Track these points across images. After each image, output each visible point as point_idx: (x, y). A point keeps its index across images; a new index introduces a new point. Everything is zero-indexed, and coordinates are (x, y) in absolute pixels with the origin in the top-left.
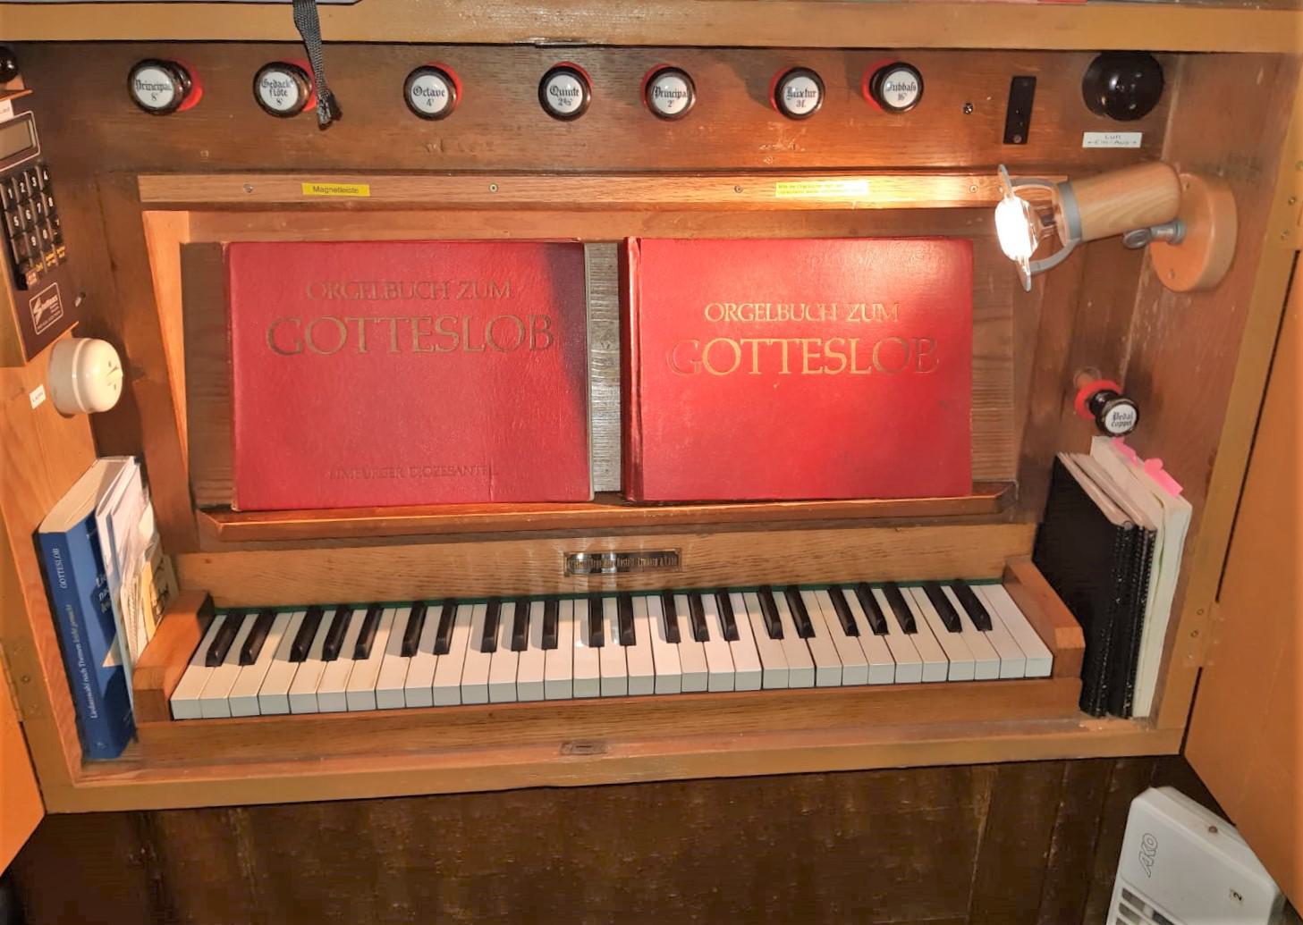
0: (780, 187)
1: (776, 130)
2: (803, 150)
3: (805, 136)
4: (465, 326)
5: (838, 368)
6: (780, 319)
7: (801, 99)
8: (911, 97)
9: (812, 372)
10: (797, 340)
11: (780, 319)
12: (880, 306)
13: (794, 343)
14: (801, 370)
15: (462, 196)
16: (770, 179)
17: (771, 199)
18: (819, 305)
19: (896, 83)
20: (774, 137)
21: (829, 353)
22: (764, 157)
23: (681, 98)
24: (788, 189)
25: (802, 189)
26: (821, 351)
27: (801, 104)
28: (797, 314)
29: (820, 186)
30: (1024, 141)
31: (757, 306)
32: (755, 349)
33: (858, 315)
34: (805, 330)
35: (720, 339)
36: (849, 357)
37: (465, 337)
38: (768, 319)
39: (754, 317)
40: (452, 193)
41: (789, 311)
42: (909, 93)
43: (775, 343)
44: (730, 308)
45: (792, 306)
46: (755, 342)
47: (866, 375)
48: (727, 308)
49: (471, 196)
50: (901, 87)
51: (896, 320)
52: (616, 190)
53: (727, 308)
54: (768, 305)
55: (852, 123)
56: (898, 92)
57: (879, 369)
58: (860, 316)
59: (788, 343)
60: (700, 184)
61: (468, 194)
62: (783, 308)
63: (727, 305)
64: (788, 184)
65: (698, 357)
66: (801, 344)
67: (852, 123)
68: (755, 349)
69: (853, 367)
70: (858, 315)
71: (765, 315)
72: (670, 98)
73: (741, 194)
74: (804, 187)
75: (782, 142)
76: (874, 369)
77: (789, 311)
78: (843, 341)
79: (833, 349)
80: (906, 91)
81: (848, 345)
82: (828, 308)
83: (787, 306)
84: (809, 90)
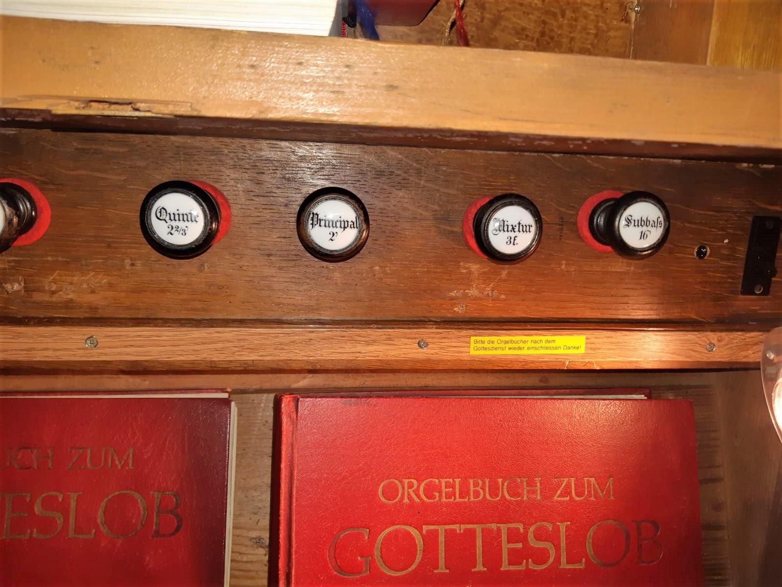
0: (476, 342)
1: (470, 273)
2: (503, 297)
3: (505, 280)
4: (73, 504)
5: (544, 562)
6: (472, 499)
7: (512, 235)
8: (655, 235)
9: (512, 568)
10: (494, 526)
11: (472, 499)
12: (593, 480)
13: (490, 530)
14: (500, 564)
15: (50, 353)
16: (464, 333)
17: (464, 357)
18: (519, 480)
19: (636, 217)
20: (466, 281)
21: (533, 543)
22: (454, 305)
23: (348, 229)
24: (486, 345)
25: (502, 345)
26: (524, 539)
27: (512, 241)
28: (494, 491)
29: (524, 342)
30: (766, 292)
31: (443, 481)
32: (442, 539)
33: (567, 492)
34: (503, 513)
35: (397, 527)
36: (558, 548)
37: (72, 520)
38: (458, 500)
39: (440, 496)
40: (34, 349)
41: (483, 489)
42: (653, 230)
43: (466, 530)
44: (411, 486)
45: (487, 481)
46: (441, 529)
47: (580, 569)
48: (406, 486)
49: (58, 353)
50: (643, 222)
51: (612, 498)
52: (262, 344)
53: (406, 486)
54: (457, 481)
55: (563, 267)
56: (640, 229)
57: (595, 561)
58: (570, 493)
59: (483, 530)
60: (372, 338)
61: (55, 350)
62: (476, 485)
63: (406, 481)
64: (486, 339)
65: (367, 552)
66: (499, 530)
67: (563, 267)
68: (442, 539)
69: (563, 559)
70: (567, 492)
71: (454, 494)
72: (332, 230)
73: (425, 350)
74: (506, 342)
75: (477, 288)
76: (588, 562)
77: (483, 489)
78: (550, 527)
79: (538, 537)
80: (649, 228)
81: (557, 530)
82: (531, 483)
83: (480, 482)
84: (523, 223)
